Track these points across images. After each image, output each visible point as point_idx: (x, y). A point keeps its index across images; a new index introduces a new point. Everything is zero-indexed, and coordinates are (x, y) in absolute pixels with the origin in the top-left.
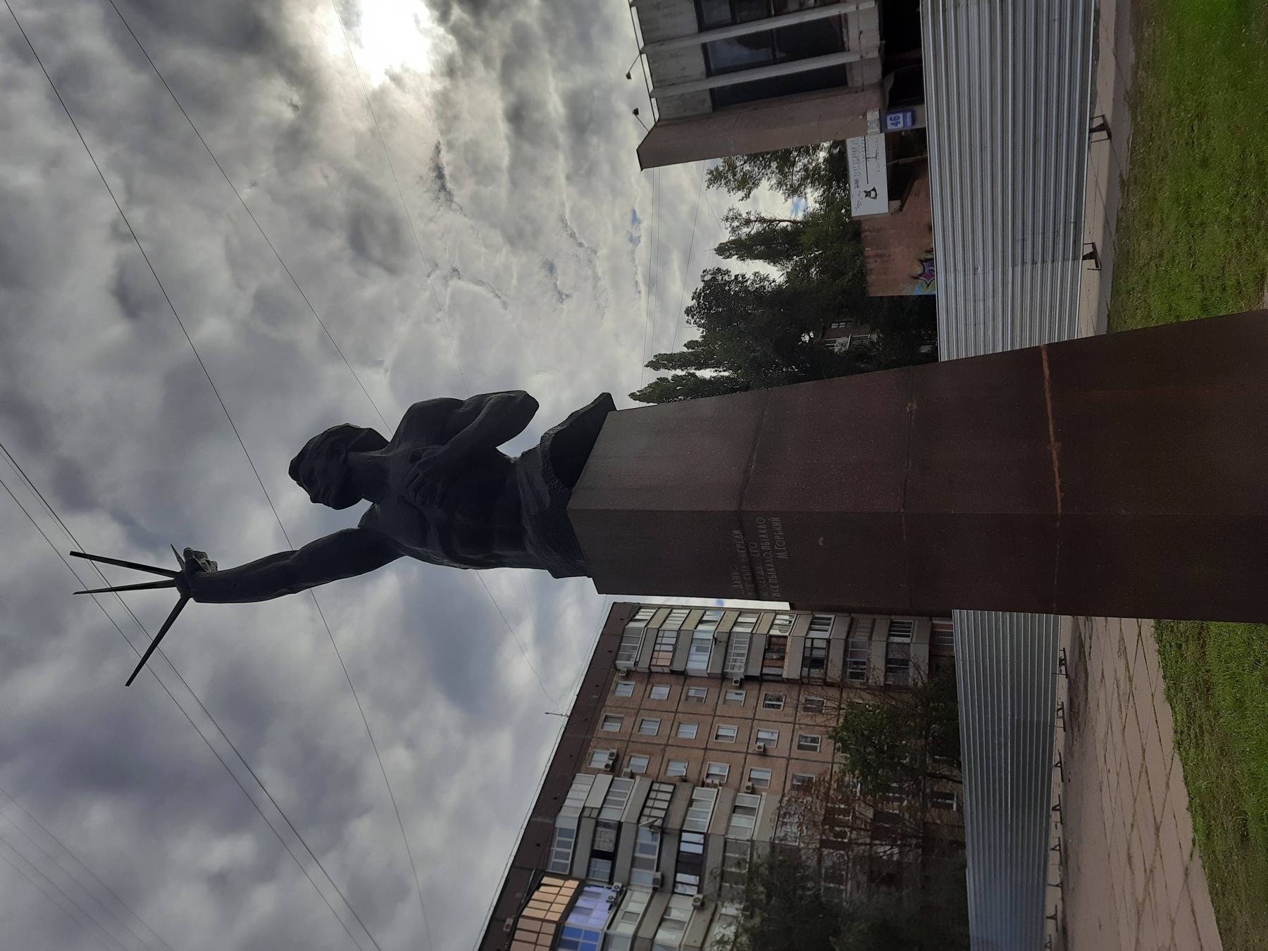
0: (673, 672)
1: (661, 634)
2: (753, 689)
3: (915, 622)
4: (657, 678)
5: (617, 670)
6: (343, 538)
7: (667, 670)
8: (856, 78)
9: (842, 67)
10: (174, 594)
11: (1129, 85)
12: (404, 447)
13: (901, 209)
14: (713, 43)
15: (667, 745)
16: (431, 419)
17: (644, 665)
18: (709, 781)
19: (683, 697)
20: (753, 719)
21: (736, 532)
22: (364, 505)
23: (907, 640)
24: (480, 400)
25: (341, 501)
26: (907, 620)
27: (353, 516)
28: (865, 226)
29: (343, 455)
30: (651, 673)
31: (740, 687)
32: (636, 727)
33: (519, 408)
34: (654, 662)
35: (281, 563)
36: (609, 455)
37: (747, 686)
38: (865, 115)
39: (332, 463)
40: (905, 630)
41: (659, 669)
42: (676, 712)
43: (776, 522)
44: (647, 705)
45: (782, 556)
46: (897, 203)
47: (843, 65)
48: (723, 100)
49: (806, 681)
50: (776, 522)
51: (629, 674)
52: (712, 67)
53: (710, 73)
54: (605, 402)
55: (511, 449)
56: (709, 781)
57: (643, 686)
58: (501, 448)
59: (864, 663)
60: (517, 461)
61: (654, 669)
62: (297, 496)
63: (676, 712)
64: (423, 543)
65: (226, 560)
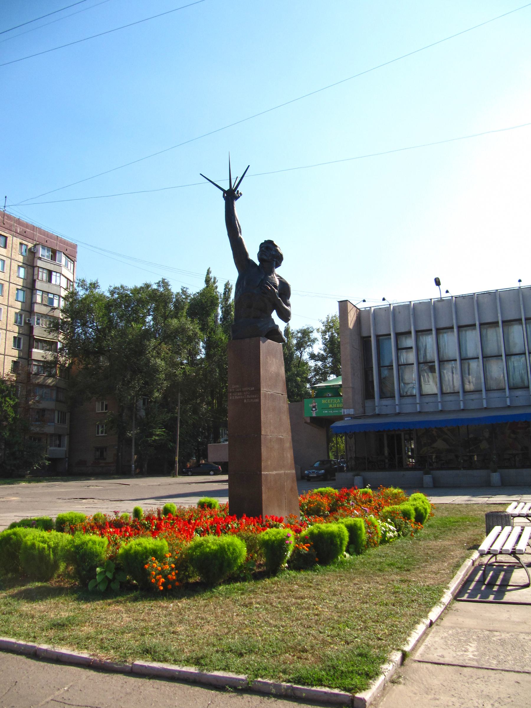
1: (58, 275)
3: (66, 426)
4: (30, 271)
6: (246, 254)
7: (35, 277)
8: (368, 403)
9: (373, 398)
10: (227, 188)
13: (306, 423)
14: (390, 338)
20: (6, 330)
21: (253, 388)
23: (56, 422)
25: (260, 259)
26: (67, 421)
27: (253, 255)
31: (25, 323)
33: (285, 316)
34: (40, 270)
37: (26, 327)
39: (271, 253)
40: (62, 420)
41: (36, 272)
42: (10, 282)
45: (245, 401)
46: (309, 421)
47: (374, 398)
48: (365, 342)
52: (381, 338)
53: (377, 336)
55: (274, 315)
58: (275, 312)
60: (271, 316)
61: (36, 269)
63: (10, 282)
65: (237, 205)
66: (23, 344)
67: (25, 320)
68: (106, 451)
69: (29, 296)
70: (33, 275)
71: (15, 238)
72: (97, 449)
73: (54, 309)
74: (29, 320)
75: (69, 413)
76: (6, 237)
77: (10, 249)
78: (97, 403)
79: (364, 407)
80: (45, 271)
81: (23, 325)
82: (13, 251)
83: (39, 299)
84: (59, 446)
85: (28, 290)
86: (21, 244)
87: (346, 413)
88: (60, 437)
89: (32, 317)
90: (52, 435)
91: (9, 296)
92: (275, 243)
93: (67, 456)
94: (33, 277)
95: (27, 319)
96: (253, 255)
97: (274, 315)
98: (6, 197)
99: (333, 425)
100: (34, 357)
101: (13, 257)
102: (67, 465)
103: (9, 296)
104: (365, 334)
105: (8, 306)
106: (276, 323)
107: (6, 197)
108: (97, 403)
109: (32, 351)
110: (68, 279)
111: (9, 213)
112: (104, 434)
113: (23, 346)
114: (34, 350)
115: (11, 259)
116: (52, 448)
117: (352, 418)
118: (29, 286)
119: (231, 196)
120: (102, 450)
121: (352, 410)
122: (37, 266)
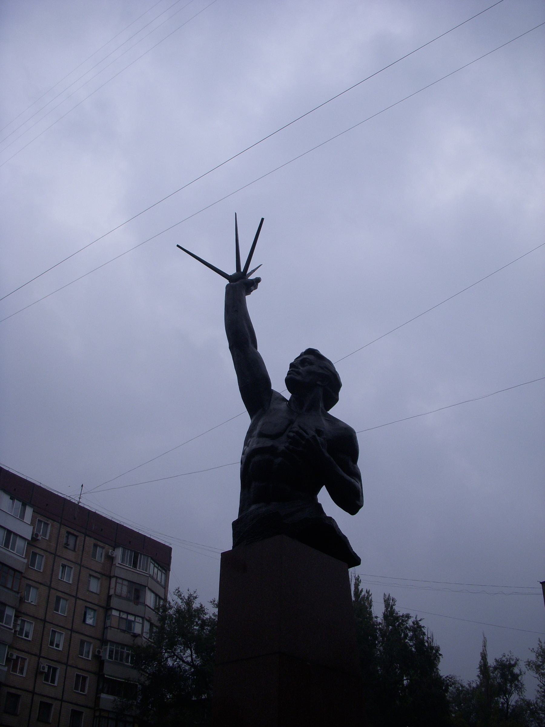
0: (109, 597)
6: (264, 380)
7: (112, 592)
10: (231, 270)
12: (325, 424)
15: (50, 587)
16: (345, 443)
17: (117, 572)
18: (19, 622)
22: (287, 395)
24: (357, 476)
25: (290, 382)
27: (279, 385)
30: (110, 577)
31: (94, 656)
34: (120, 581)
35: (250, 341)
39: (316, 377)
54: (355, 561)
55: (324, 497)
56: (19, 622)
58: (324, 490)
60: (316, 500)
61: (113, 580)
62: (293, 354)
65: (252, 302)
67: (93, 653)
73: (135, 636)
74: (99, 652)
76: (77, 537)
80: (126, 583)
83: (114, 622)
94: (109, 593)
95: (97, 649)
97: (324, 497)
98: (82, 486)
107: (82, 486)
109: (100, 697)
119: (240, 285)
122: (114, 576)
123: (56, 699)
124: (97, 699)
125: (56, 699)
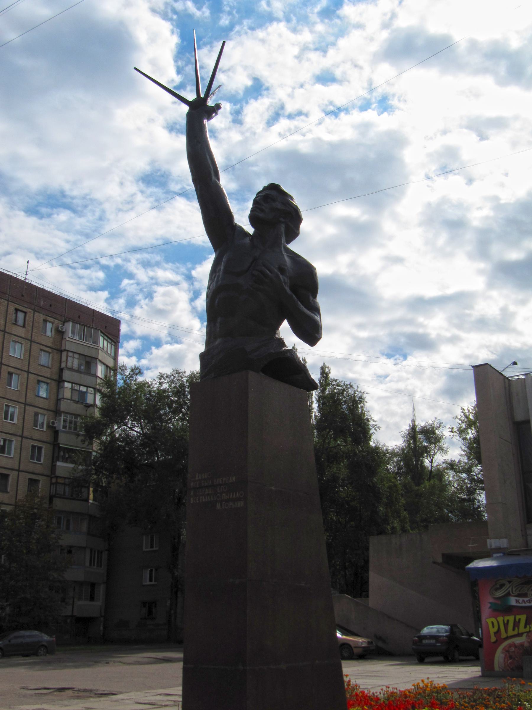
0: (61, 370)
2: (48, 437)
5: (64, 323)
7: (63, 365)
10: (191, 97)
11: (22, 494)
19: (41, 378)
21: (234, 479)
22: (250, 229)
25: (253, 219)
27: (242, 218)
28: (417, 661)
29: (283, 220)
30: (61, 351)
31: (48, 427)
32: (15, 338)
33: (311, 333)
34: (70, 354)
35: (213, 173)
36: (279, 390)
38: (506, 538)
39: (277, 212)
42: (28, 372)
43: (241, 504)
44: (35, 347)
45: (218, 506)
46: (440, 560)
49: (54, 480)
50: (241, 504)
51: (60, 333)
55: (286, 332)
57: (50, 344)
58: (285, 325)
59: (68, 528)
61: (64, 354)
64: (226, 271)
66: (45, 456)
68: (155, 607)
69: (55, 391)
70: (61, 362)
71: (37, 314)
72: (144, 604)
74: (53, 423)
75: (106, 552)
76: (25, 313)
77: (30, 328)
78: (144, 537)
79: (525, 536)
80: (76, 356)
81: (45, 429)
82: (35, 331)
83: (67, 394)
84: (92, 598)
85: (53, 383)
86: (17, 310)
87: (493, 547)
88: (93, 585)
89: (58, 418)
90: (81, 584)
91: (26, 391)
92: (283, 188)
93: (103, 614)
96: (242, 218)
97: (286, 332)
99: (472, 565)
100: (58, 473)
101: (35, 338)
102: (102, 628)
103: (26, 391)
104: (519, 417)
105: (25, 404)
106: (289, 345)
107: (28, 262)
108: (144, 537)
109: (55, 465)
110: (107, 366)
111: (30, 282)
112: (153, 583)
113: (44, 460)
114: (59, 464)
115: (31, 341)
116: (81, 603)
117: (504, 554)
118: (55, 377)
120: (150, 607)
121: (505, 540)
122: (65, 350)
123: (12, 469)
124: (53, 467)
125: (12, 469)
